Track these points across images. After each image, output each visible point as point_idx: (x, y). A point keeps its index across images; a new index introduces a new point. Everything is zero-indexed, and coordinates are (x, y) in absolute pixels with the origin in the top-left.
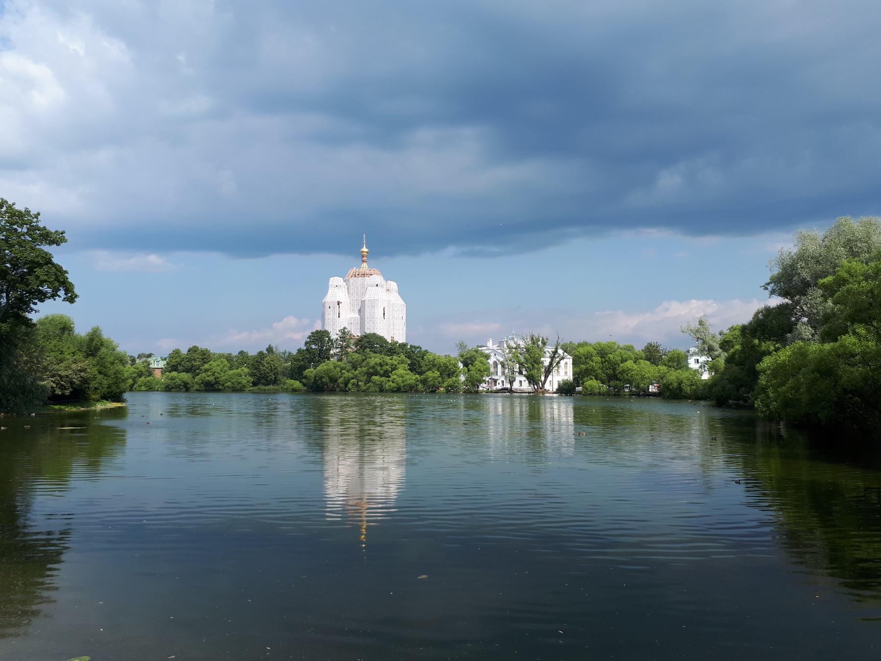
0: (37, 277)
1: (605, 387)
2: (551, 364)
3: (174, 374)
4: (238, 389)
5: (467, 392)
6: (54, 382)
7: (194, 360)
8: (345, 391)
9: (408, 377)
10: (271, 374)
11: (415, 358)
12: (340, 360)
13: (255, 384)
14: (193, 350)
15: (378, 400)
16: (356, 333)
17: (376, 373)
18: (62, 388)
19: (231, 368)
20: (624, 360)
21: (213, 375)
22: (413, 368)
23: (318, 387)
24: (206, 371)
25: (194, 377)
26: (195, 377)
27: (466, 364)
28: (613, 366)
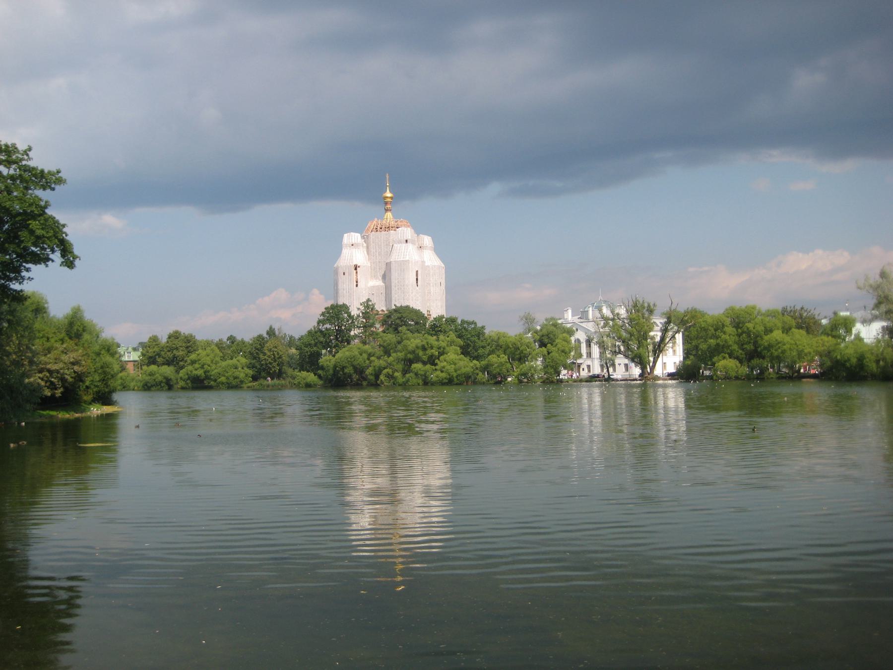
0: (32, 232)
1: (745, 370)
2: (663, 339)
3: (153, 368)
4: (234, 385)
5: (547, 382)
6: (42, 379)
7: (177, 349)
8: (375, 385)
9: (462, 363)
10: (275, 364)
11: (471, 340)
12: (364, 343)
13: (255, 378)
14: (175, 336)
15: (418, 396)
16: (381, 306)
17: (417, 359)
18: (52, 386)
19: (223, 359)
20: (769, 331)
21: (202, 367)
22: (465, 351)
23: (338, 380)
24: (193, 362)
25: (177, 372)
26: (179, 369)
27: (543, 344)
28: (755, 339)
